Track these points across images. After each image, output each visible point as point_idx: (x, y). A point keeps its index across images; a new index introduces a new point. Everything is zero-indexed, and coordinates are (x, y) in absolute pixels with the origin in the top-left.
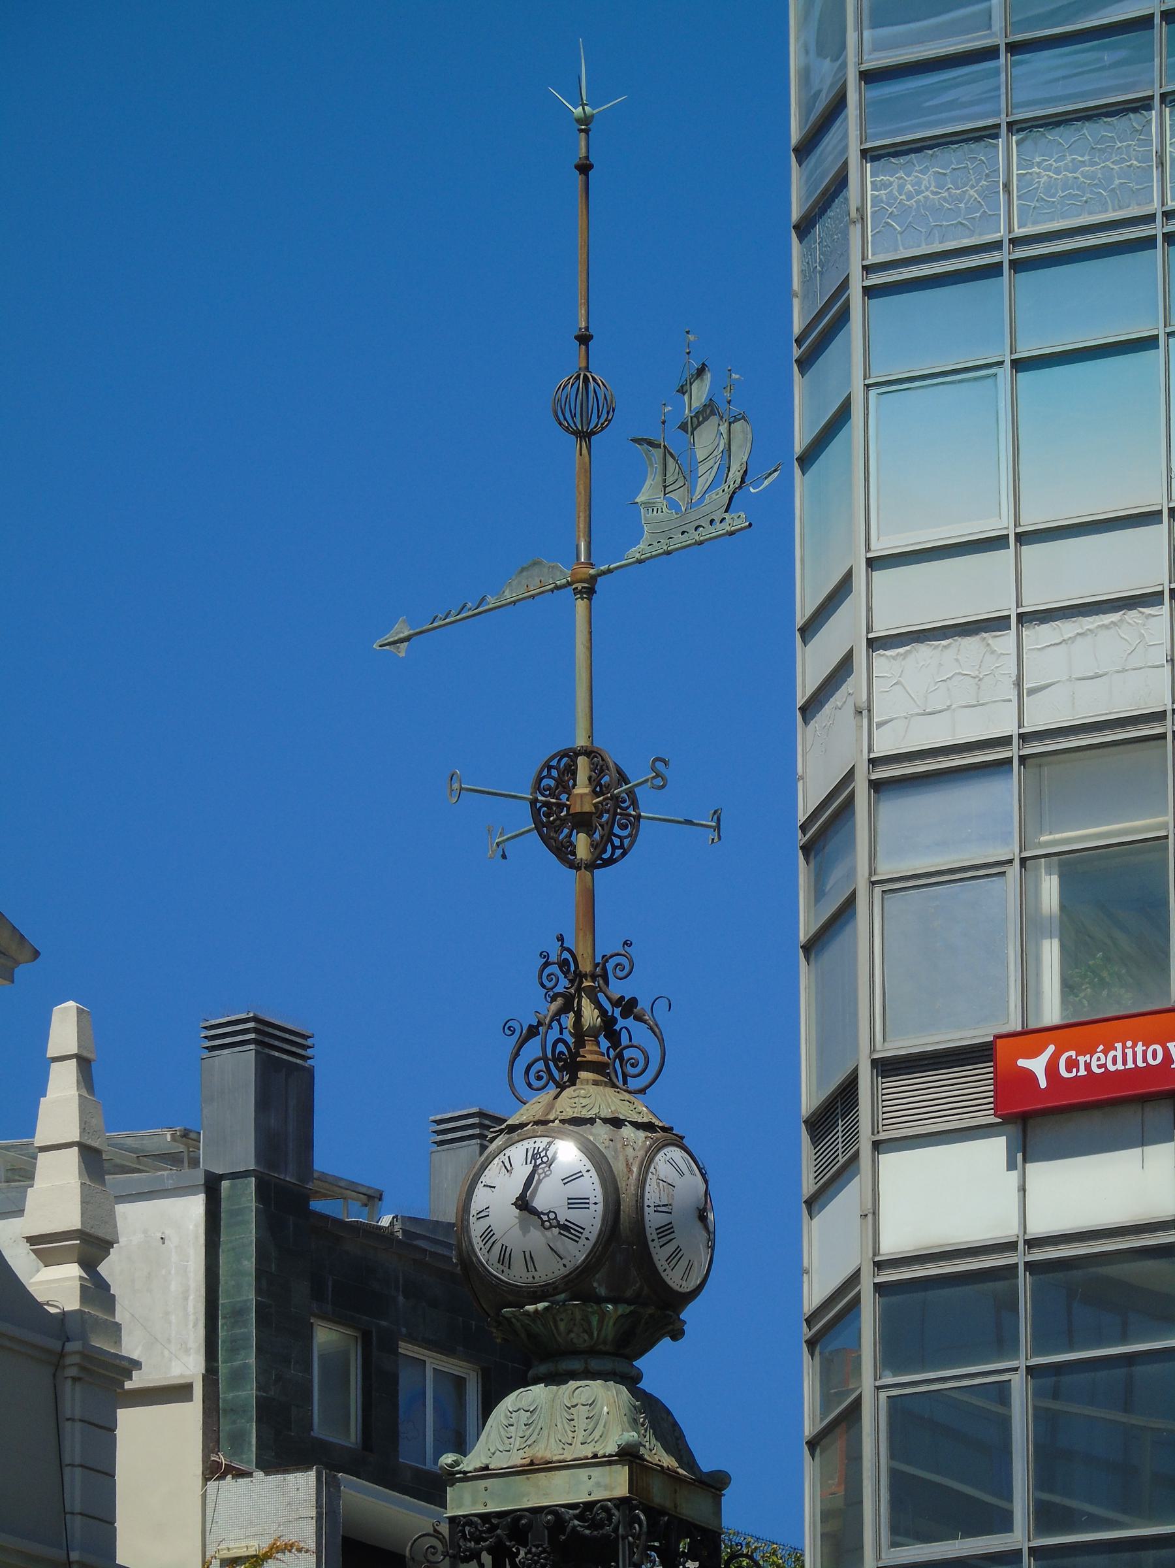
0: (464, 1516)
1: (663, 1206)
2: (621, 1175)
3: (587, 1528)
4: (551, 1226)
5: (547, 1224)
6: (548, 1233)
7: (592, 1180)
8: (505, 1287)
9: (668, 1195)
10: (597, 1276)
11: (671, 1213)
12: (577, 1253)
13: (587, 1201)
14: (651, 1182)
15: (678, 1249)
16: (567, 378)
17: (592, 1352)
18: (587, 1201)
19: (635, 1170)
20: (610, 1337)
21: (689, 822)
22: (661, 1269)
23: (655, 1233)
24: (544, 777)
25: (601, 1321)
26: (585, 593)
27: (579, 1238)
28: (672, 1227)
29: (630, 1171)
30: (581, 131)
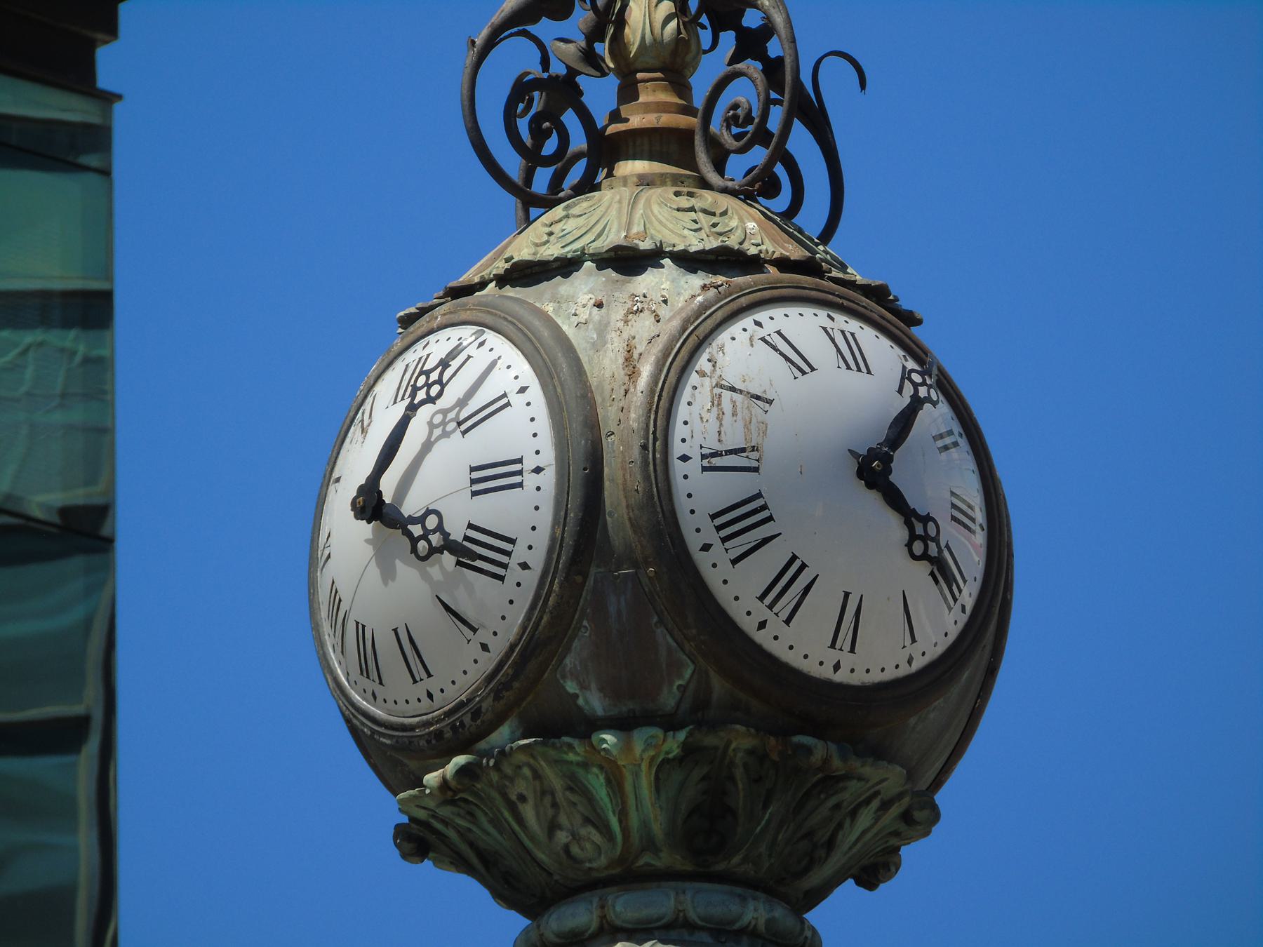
1: (730, 452)
2: (607, 388)
4: (433, 551)
5: (422, 545)
6: (434, 571)
7: (531, 412)
8: (384, 735)
10: (569, 661)
11: (756, 470)
13: (517, 467)
14: (693, 395)
15: (793, 567)
18: (517, 467)
19: (646, 370)
20: (658, 829)
22: (748, 625)
23: (708, 527)
25: (615, 782)
27: (505, 566)
28: (473, 482)
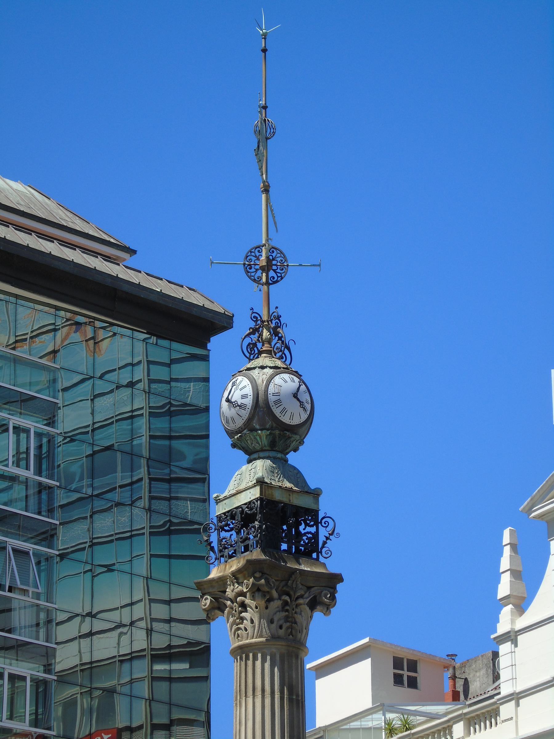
0: (219, 515)
3: (249, 511)
4: (236, 406)
5: (235, 406)
6: (236, 409)
7: (249, 388)
9: (278, 390)
10: (254, 421)
12: (245, 414)
16: (256, 122)
17: (262, 450)
19: (265, 382)
20: (266, 444)
21: (300, 265)
22: (278, 417)
24: (249, 256)
25: (260, 438)
26: (264, 191)
29: (263, 383)
30: (263, 38)
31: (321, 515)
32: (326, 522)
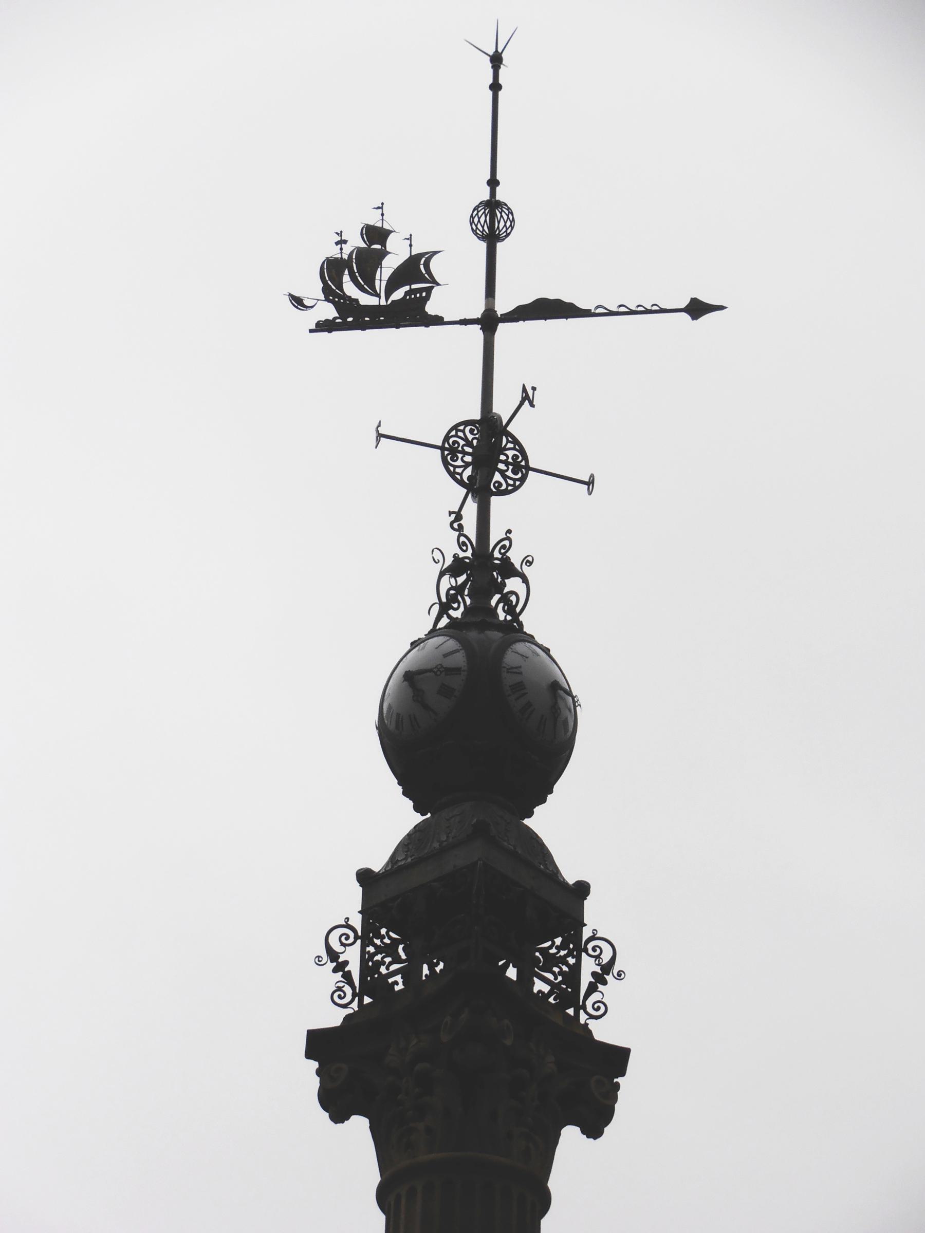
5: (438, 673)
31: (586, 933)
32: (596, 1006)
